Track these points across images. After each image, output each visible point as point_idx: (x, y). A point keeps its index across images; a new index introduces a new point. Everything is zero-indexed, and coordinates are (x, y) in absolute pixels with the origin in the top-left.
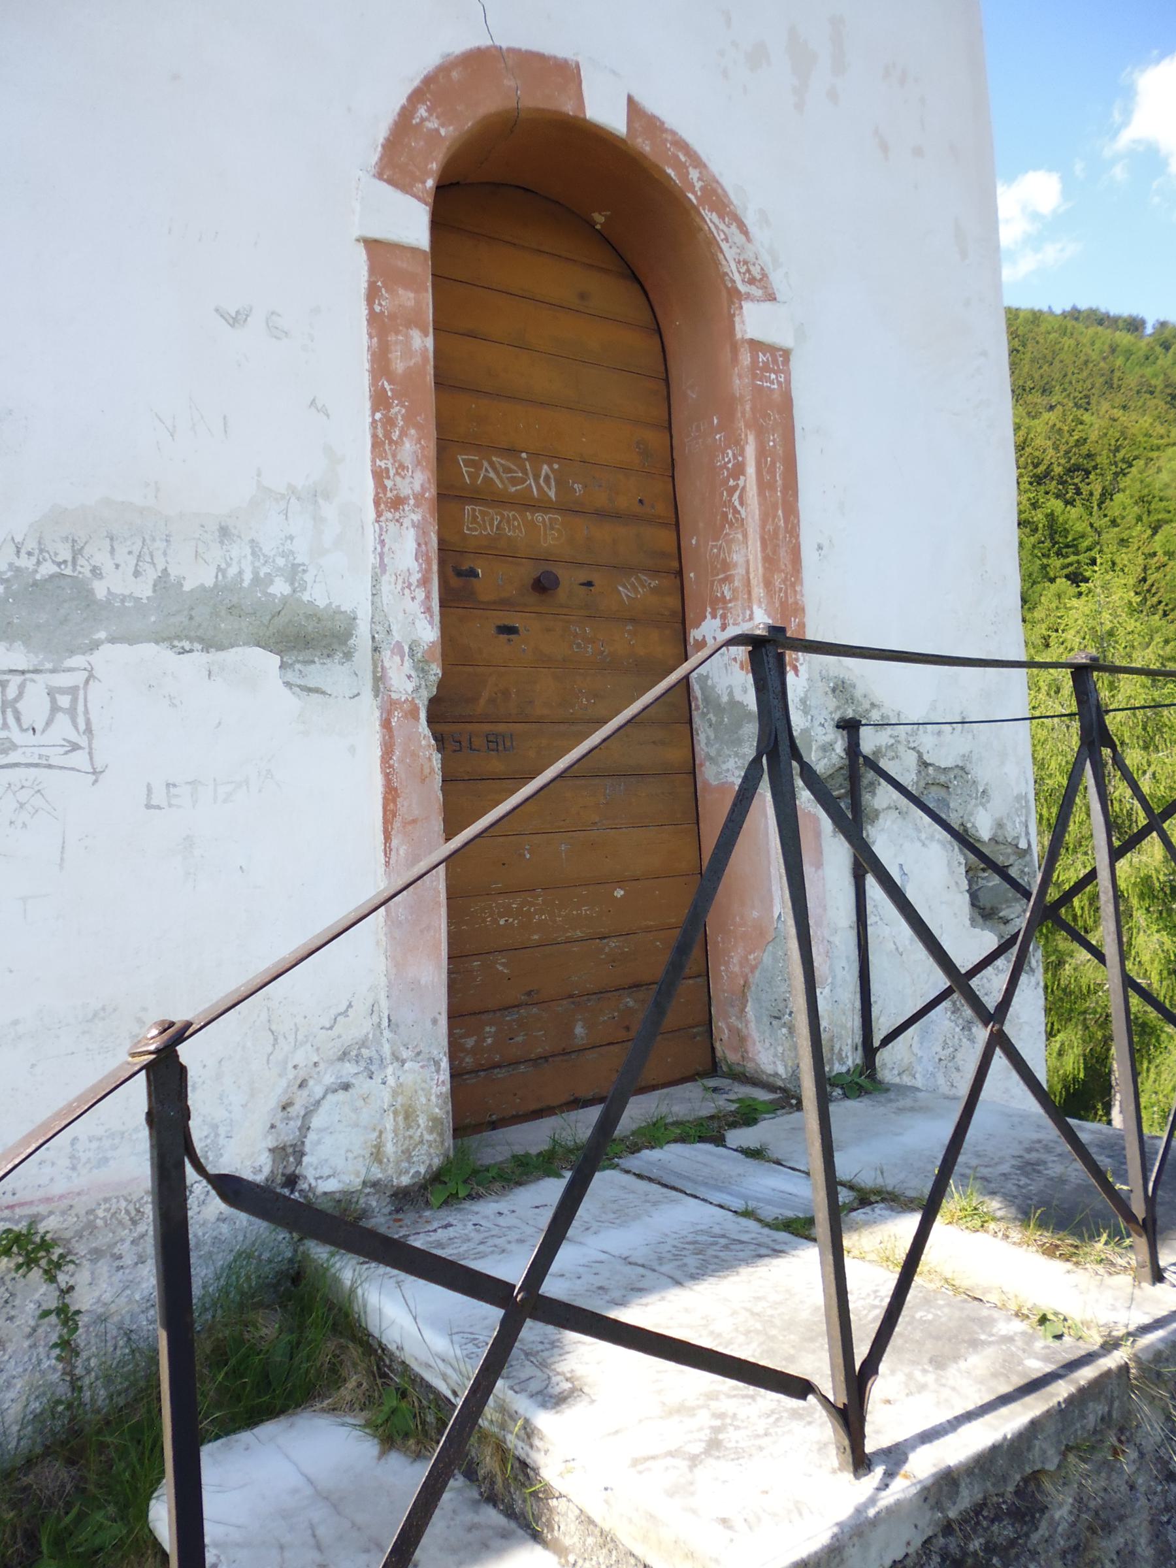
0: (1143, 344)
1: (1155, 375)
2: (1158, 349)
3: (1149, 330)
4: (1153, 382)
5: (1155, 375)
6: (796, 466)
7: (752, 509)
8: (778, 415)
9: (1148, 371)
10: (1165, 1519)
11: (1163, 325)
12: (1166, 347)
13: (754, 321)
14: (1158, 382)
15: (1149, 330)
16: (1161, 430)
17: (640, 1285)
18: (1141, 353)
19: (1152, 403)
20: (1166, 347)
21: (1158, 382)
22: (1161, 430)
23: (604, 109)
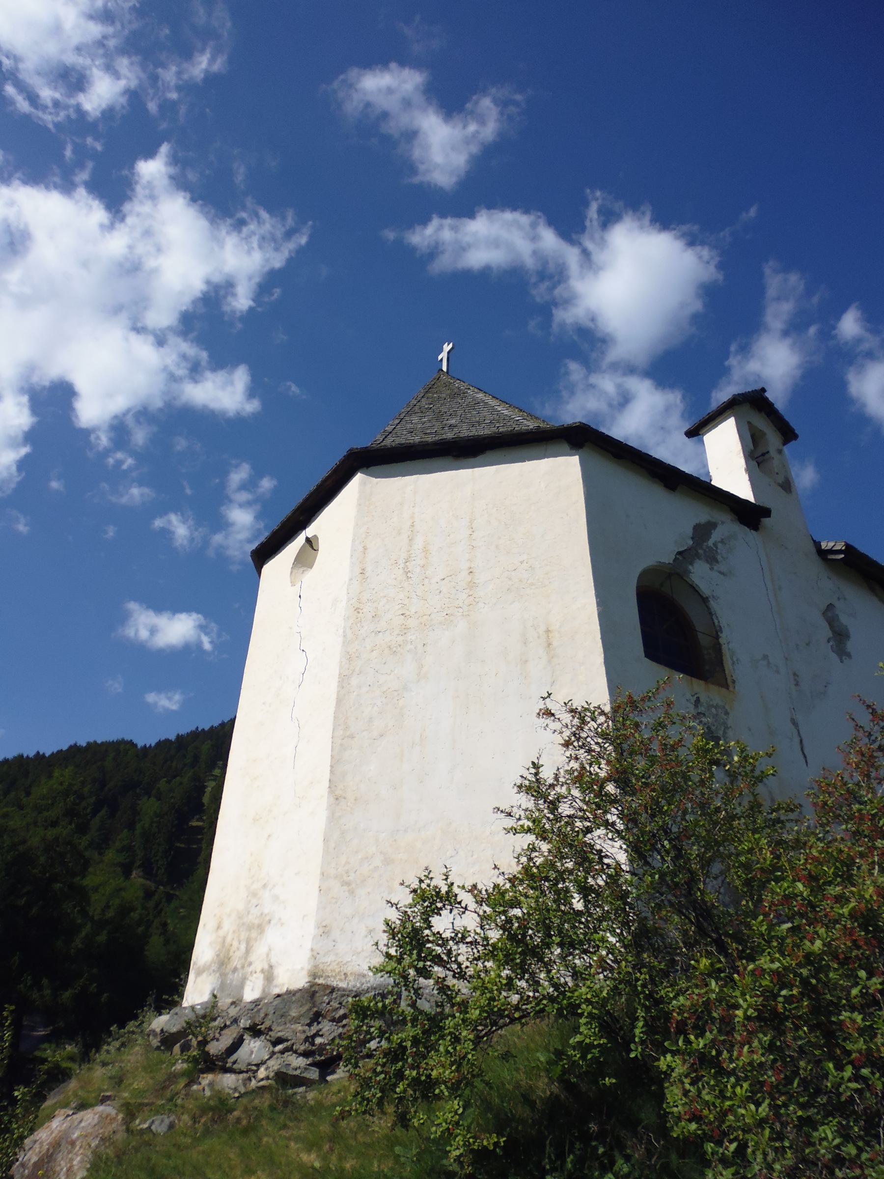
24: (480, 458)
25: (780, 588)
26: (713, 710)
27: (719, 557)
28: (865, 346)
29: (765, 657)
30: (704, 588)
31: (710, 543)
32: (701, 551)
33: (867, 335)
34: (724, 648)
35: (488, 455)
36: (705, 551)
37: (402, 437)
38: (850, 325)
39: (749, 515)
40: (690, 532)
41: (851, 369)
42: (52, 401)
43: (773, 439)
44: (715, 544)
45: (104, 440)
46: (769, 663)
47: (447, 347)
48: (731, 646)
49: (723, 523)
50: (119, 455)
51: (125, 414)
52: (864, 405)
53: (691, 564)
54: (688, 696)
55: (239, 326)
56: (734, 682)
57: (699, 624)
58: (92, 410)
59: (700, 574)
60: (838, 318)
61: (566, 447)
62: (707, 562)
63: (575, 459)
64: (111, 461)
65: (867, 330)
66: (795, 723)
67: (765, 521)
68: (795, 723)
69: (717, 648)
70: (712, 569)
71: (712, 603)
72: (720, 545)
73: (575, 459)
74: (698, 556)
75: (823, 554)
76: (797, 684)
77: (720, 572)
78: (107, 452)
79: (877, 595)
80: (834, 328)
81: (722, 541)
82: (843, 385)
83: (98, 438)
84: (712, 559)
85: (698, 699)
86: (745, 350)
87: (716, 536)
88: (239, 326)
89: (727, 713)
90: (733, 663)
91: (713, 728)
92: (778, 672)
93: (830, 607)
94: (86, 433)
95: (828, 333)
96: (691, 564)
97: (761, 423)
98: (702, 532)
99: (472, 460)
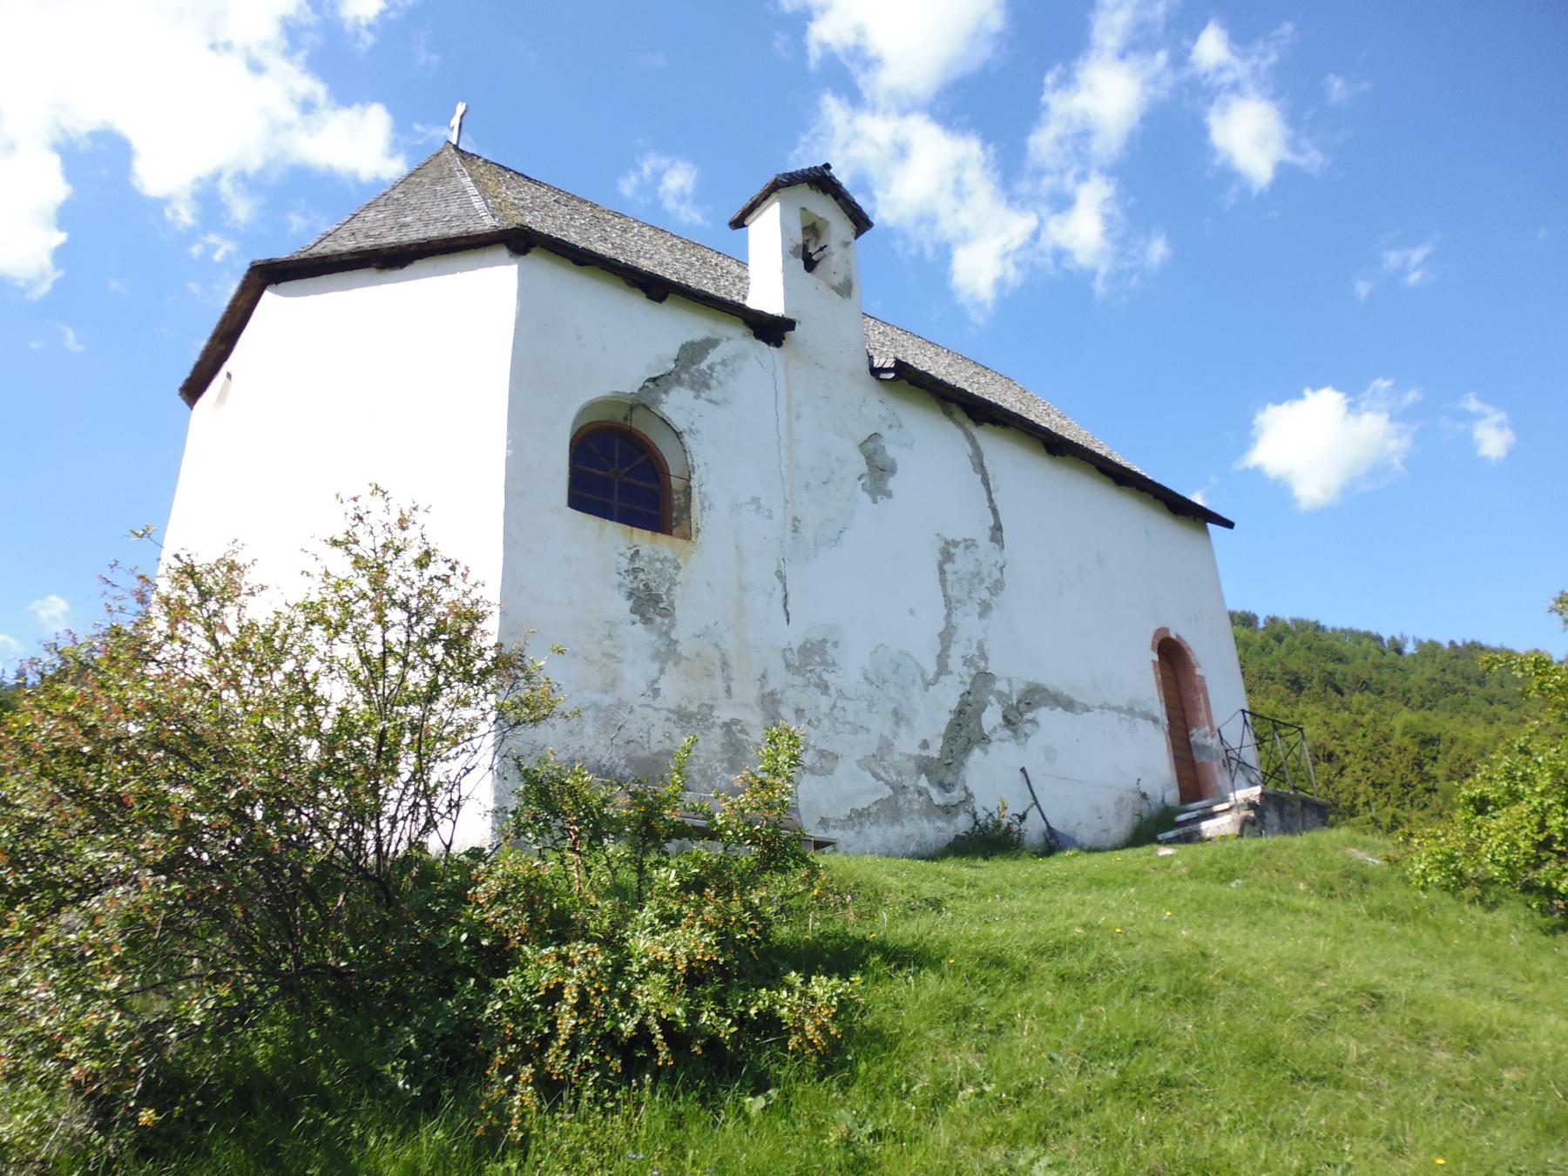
0: (1258, 637)
1: (1273, 664)
2: (1272, 642)
3: (1261, 625)
4: (1272, 670)
5: (1273, 664)
6: (516, 347)
7: (1203, 707)
8: (1204, 690)
9: (1266, 660)
10: (1192, 1069)
11: (1273, 620)
12: (1279, 639)
13: (1198, 672)
14: (1277, 670)
15: (1261, 625)
16: (1286, 711)
17: (1317, 790)
18: (1258, 645)
19: (1273, 688)
20: (1279, 639)
21: (1277, 670)
22: (1286, 711)
23: (1173, 636)
24: (408, 269)
25: (798, 417)
26: (658, 565)
27: (713, 383)
28: (1228, 77)
29: (755, 500)
30: (678, 421)
31: (703, 366)
32: (684, 376)
33: (1235, 61)
34: (695, 491)
35: (417, 266)
36: (692, 375)
37: (415, 233)
38: (1211, 47)
39: (771, 330)
40: (673, 351)
41: (1212, 109)
42: (97, 163)
43: (838, 226)
44: (711, 367)
45: (185, 216)
46: (759, 507)
47: (460, 108)
48: (703, 489)
49: (729, 339)
50: (213, 239)
51: (218, 175)
52: (1230, 158)
53: (666, 392)
54: (623, 549)
55: (370, 39)
56: (698, 530)
57: (674, 468)
58: (164, 173)
59: (676, 405)
60: (1195, 37)
61: (503, 253)
62: (692, 388)
63: (515, 267)
64: (196, 250)
65: (1235, 53)
66: (780, 575)
67: (789, 334)
68: (780, 575)
69: (687, 491)
70: (697, 397)
71: (686, 438)
72: (718, 368)
73: (515, 267)
74: (679, 381)
75: (875, 372)
76: (796, 530)
77: (710, 401)
78: (191, 236)
79: (954, 420)
80: (1189, 52)
81: (723, 363)
82: (1203, 131)
83: (176, 213)
84: (701, 384)
85: (637, 552)
86: (1067, 81)
87: (714, 356)
88: (370, 39)
89: (678, 567)
90: (703, 509)
91: (653, 585)
92: (770, 517)
93: (875, 436)
94: (159, 204)
95: (1180, 59)
96: (666, 392)
97: (823, 208)
98: (692, 353)
99: (397, 273)
